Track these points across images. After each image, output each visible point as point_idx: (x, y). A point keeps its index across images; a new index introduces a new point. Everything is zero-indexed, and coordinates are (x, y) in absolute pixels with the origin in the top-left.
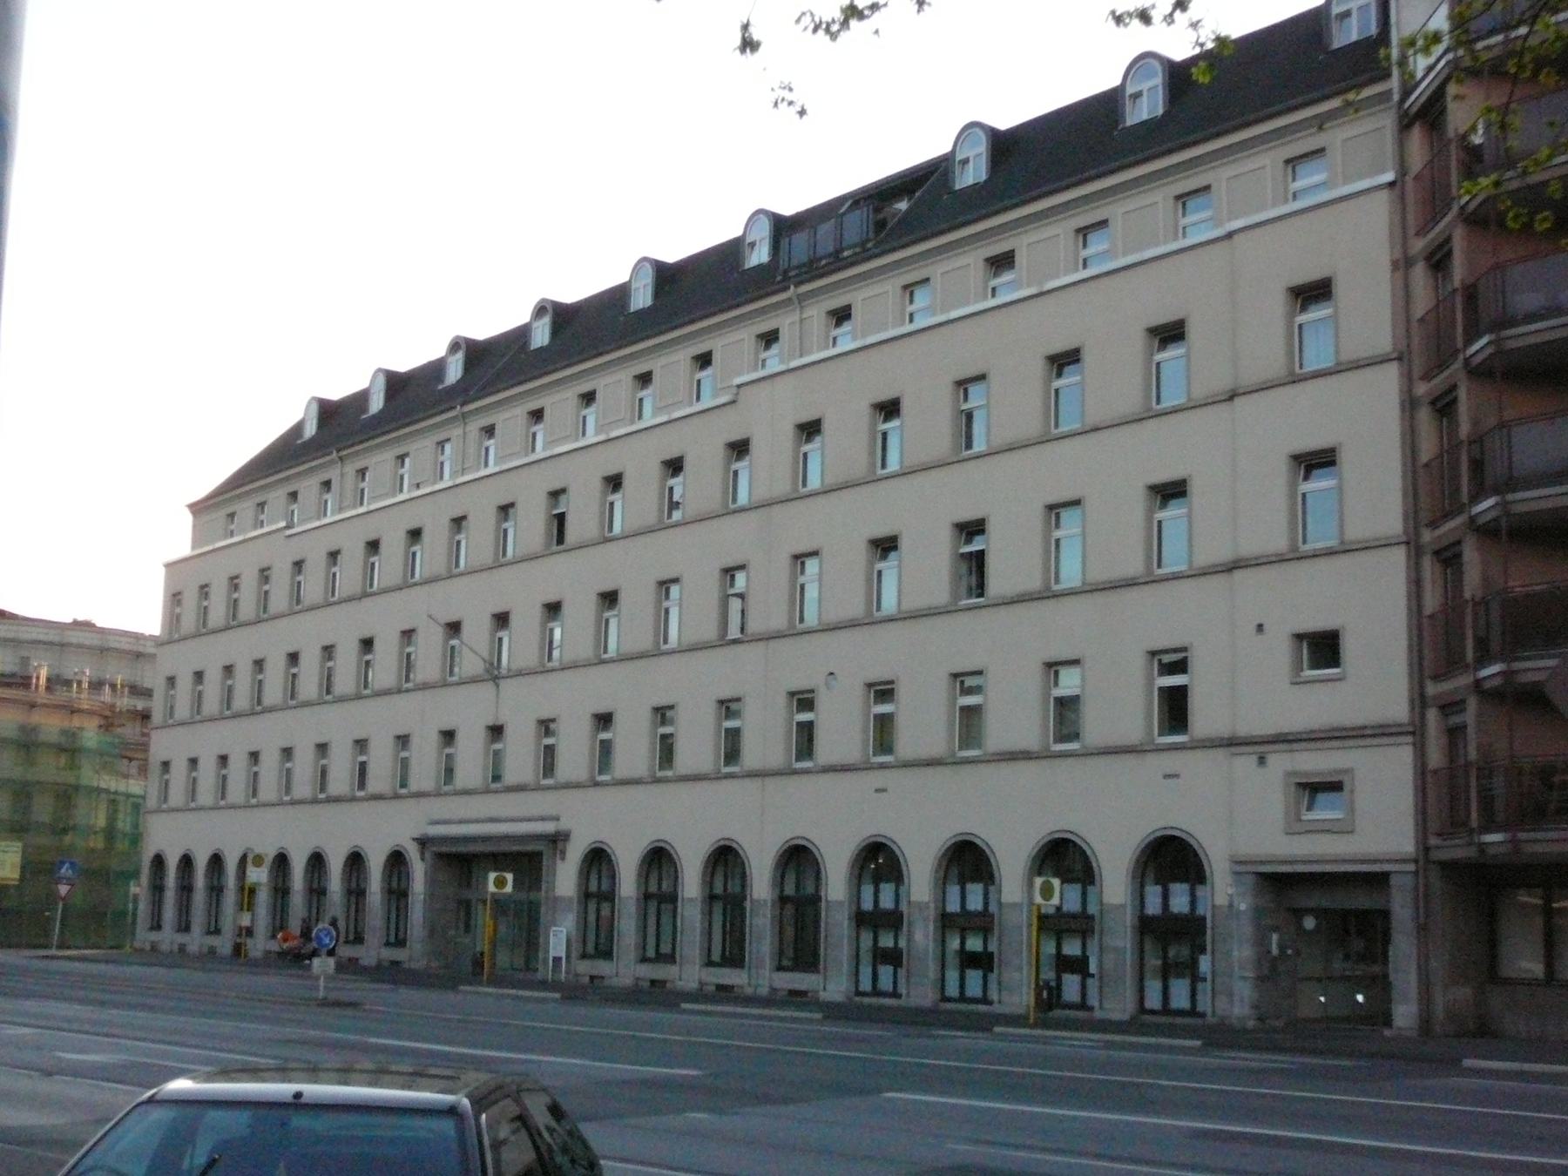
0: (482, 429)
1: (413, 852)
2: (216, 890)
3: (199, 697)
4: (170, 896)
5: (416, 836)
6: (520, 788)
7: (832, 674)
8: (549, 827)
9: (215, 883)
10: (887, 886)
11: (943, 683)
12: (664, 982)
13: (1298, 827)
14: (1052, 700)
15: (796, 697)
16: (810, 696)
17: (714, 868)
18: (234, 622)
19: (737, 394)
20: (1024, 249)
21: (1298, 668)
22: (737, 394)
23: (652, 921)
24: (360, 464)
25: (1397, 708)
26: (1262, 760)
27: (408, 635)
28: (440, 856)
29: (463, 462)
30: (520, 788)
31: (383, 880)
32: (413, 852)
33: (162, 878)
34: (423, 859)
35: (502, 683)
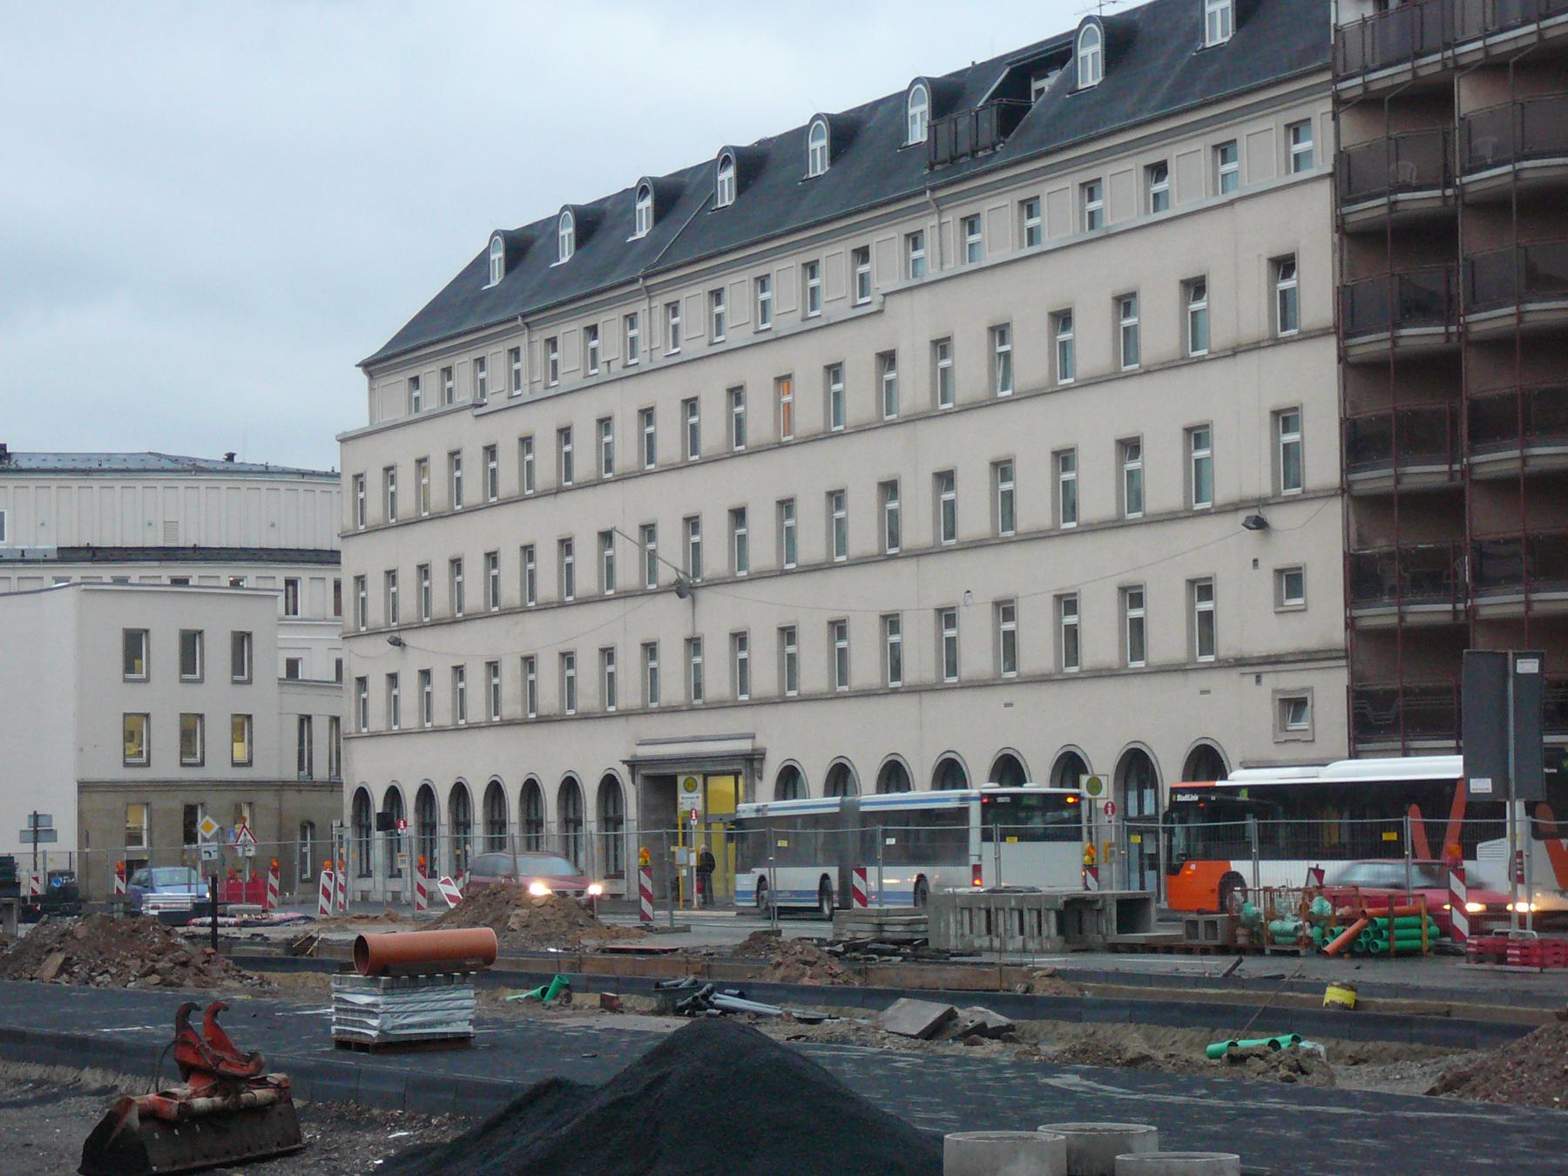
0: (855, 251)
1: (623, 775)
2: (461, 824)
5: (627, 758)
6: (673, 710)
7: (968, 592)
8: (745, 746)
9: (428, 820)
10: (1472, 786)
12: (620, 896)
13: (1284, 736)
15: (944, 614)
16: (1073, 598)
19: (884, 303)
20: (1045, 197)
22: (884, 303)
25: (1338, 636)
26: (1258, 679)
27: (606, 537)
28: (647, 778)
29: (651, 342)
30: (673, 710)
31: (559, 814)
32: (623, 775)
34: (634, 783)
35: (705, 596)
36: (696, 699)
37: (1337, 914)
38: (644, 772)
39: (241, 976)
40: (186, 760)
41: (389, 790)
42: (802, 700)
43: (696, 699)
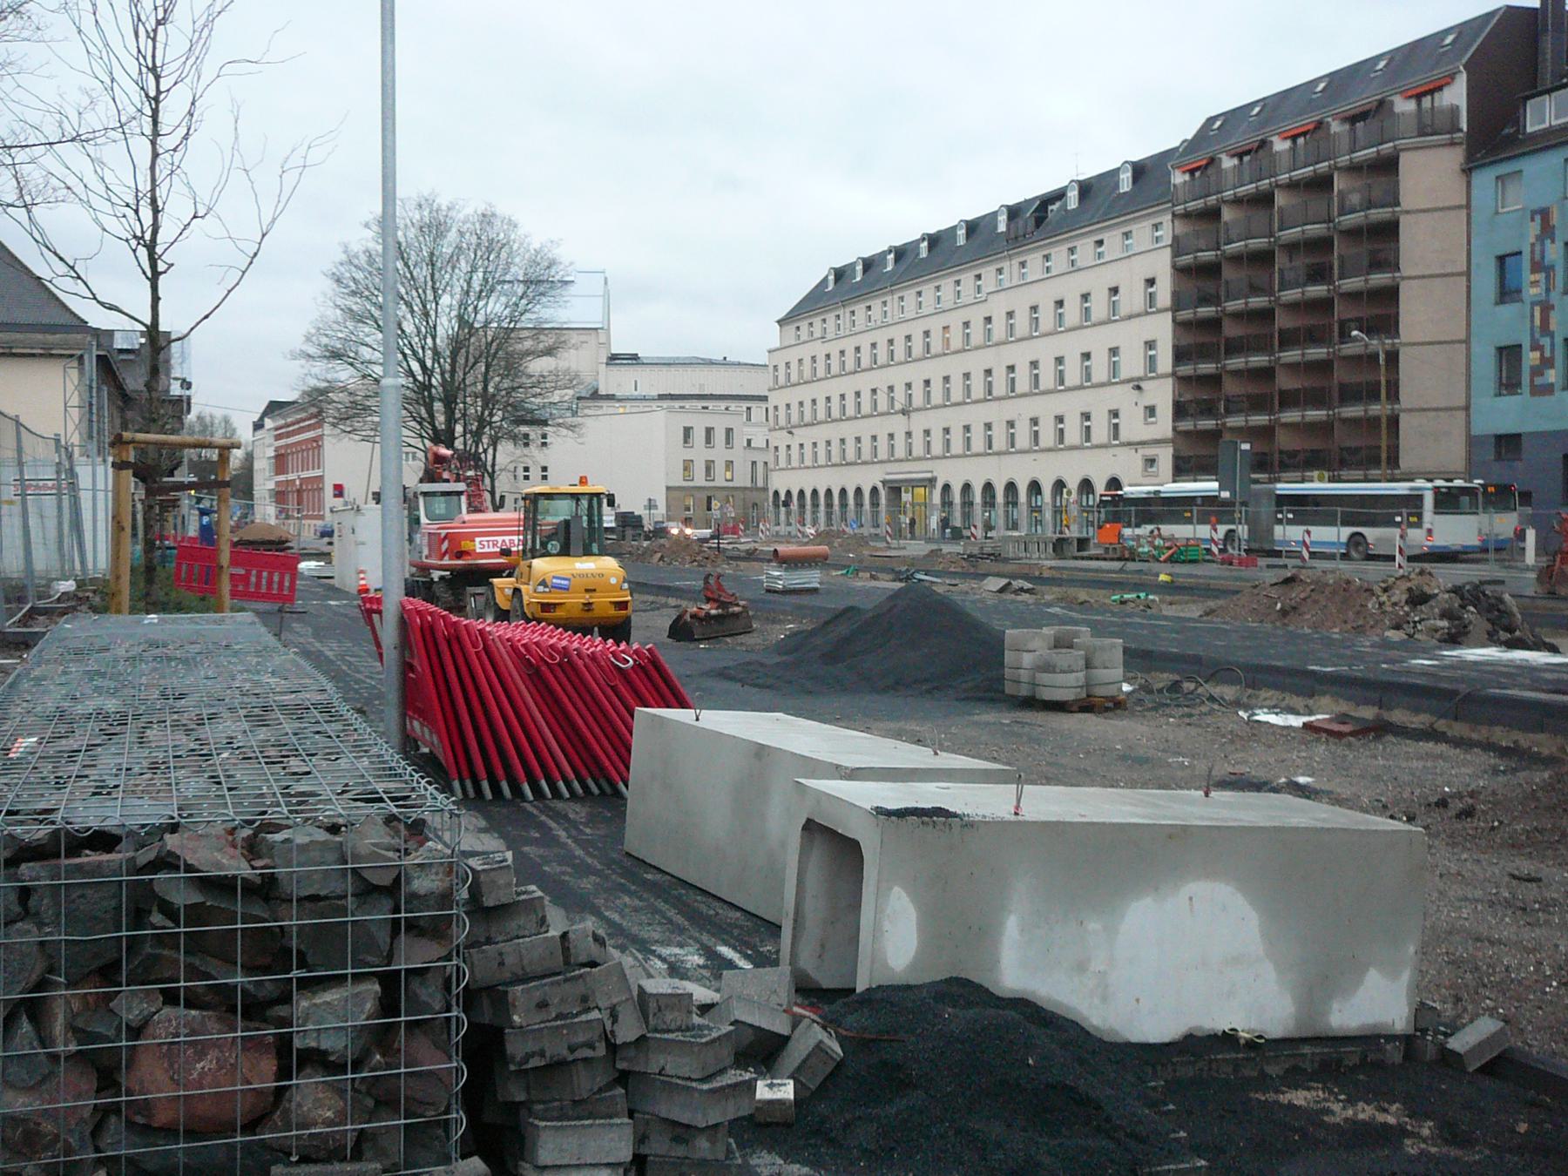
3: (777, 417)
4: (822, 508)
8: (929, 475)
11: (1106, 415)
18: (875, 365)
21: (1145, 419)
25: (1169, 434)
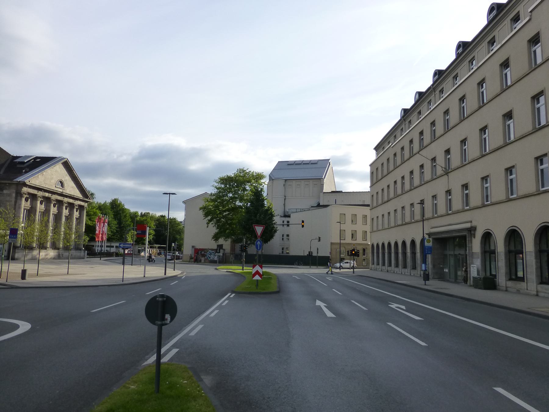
6: (458, 212)
8: (468, 225)
14: (465, 194)
17: (510, 240)
23: (488, 263)
24: (409, 120)
30: (458, 212)
31: (505, 246)
33: (415, 250)
35: (449, 174)
36: (450, 211)
37: (126, 252)
38: (432, 237)
39: (28, 227)
40: (352, 239)
41: (412, 240)
42: (438, 217)
43: (450, 211)
